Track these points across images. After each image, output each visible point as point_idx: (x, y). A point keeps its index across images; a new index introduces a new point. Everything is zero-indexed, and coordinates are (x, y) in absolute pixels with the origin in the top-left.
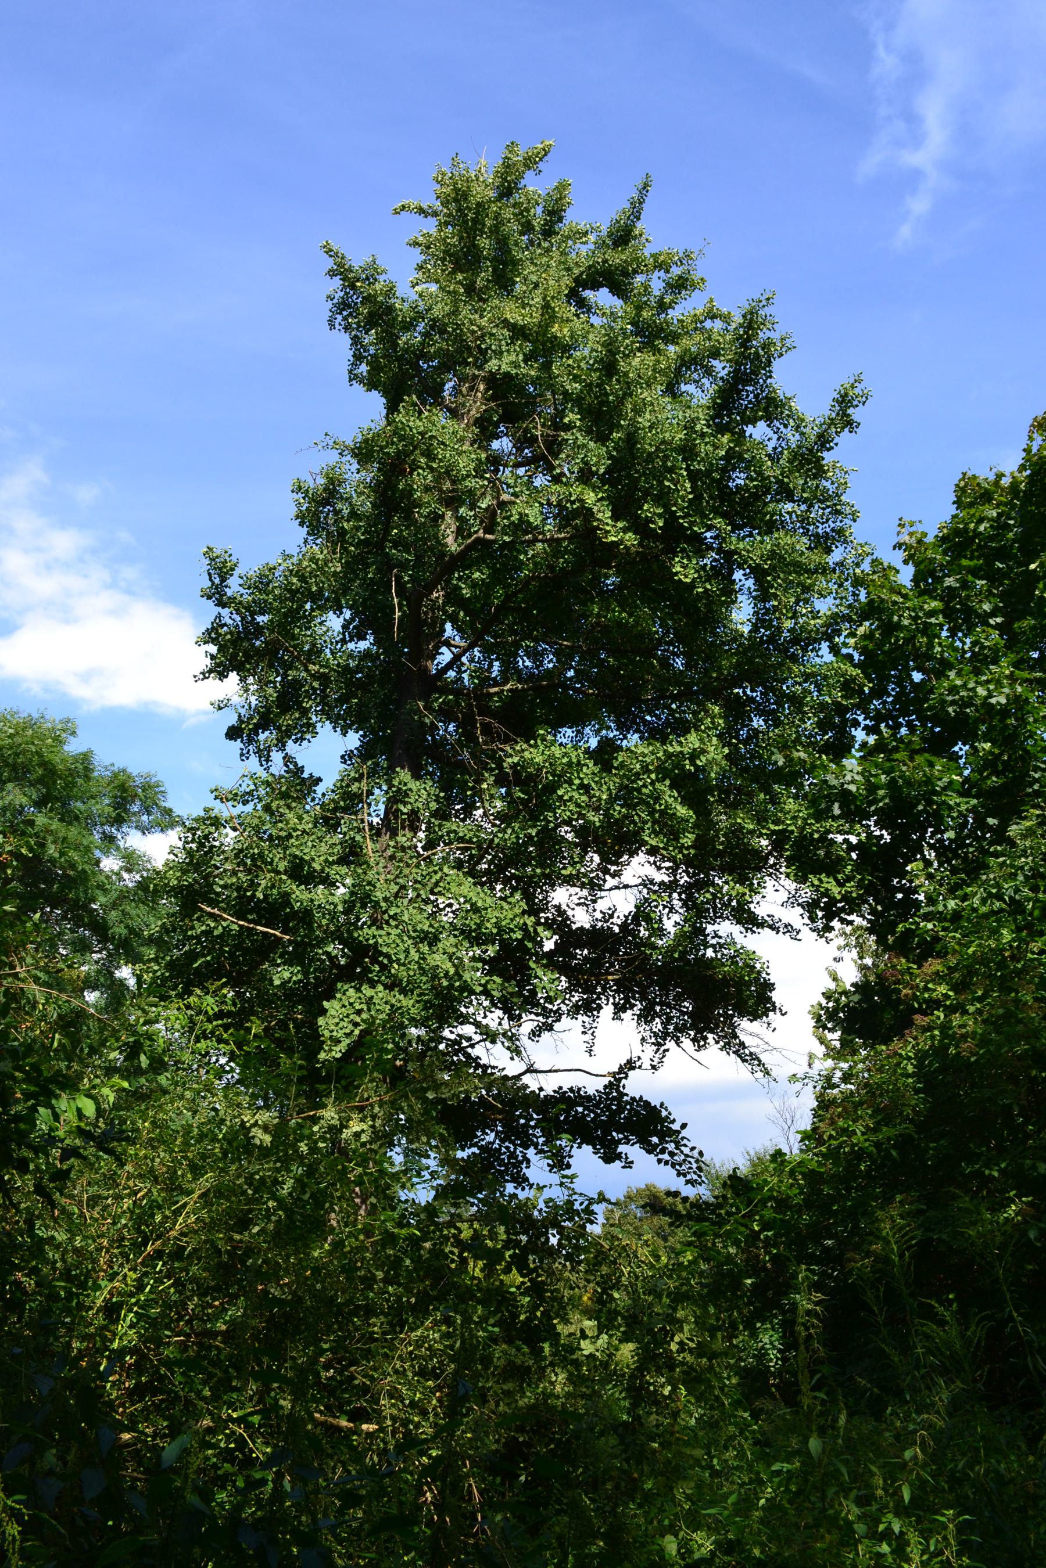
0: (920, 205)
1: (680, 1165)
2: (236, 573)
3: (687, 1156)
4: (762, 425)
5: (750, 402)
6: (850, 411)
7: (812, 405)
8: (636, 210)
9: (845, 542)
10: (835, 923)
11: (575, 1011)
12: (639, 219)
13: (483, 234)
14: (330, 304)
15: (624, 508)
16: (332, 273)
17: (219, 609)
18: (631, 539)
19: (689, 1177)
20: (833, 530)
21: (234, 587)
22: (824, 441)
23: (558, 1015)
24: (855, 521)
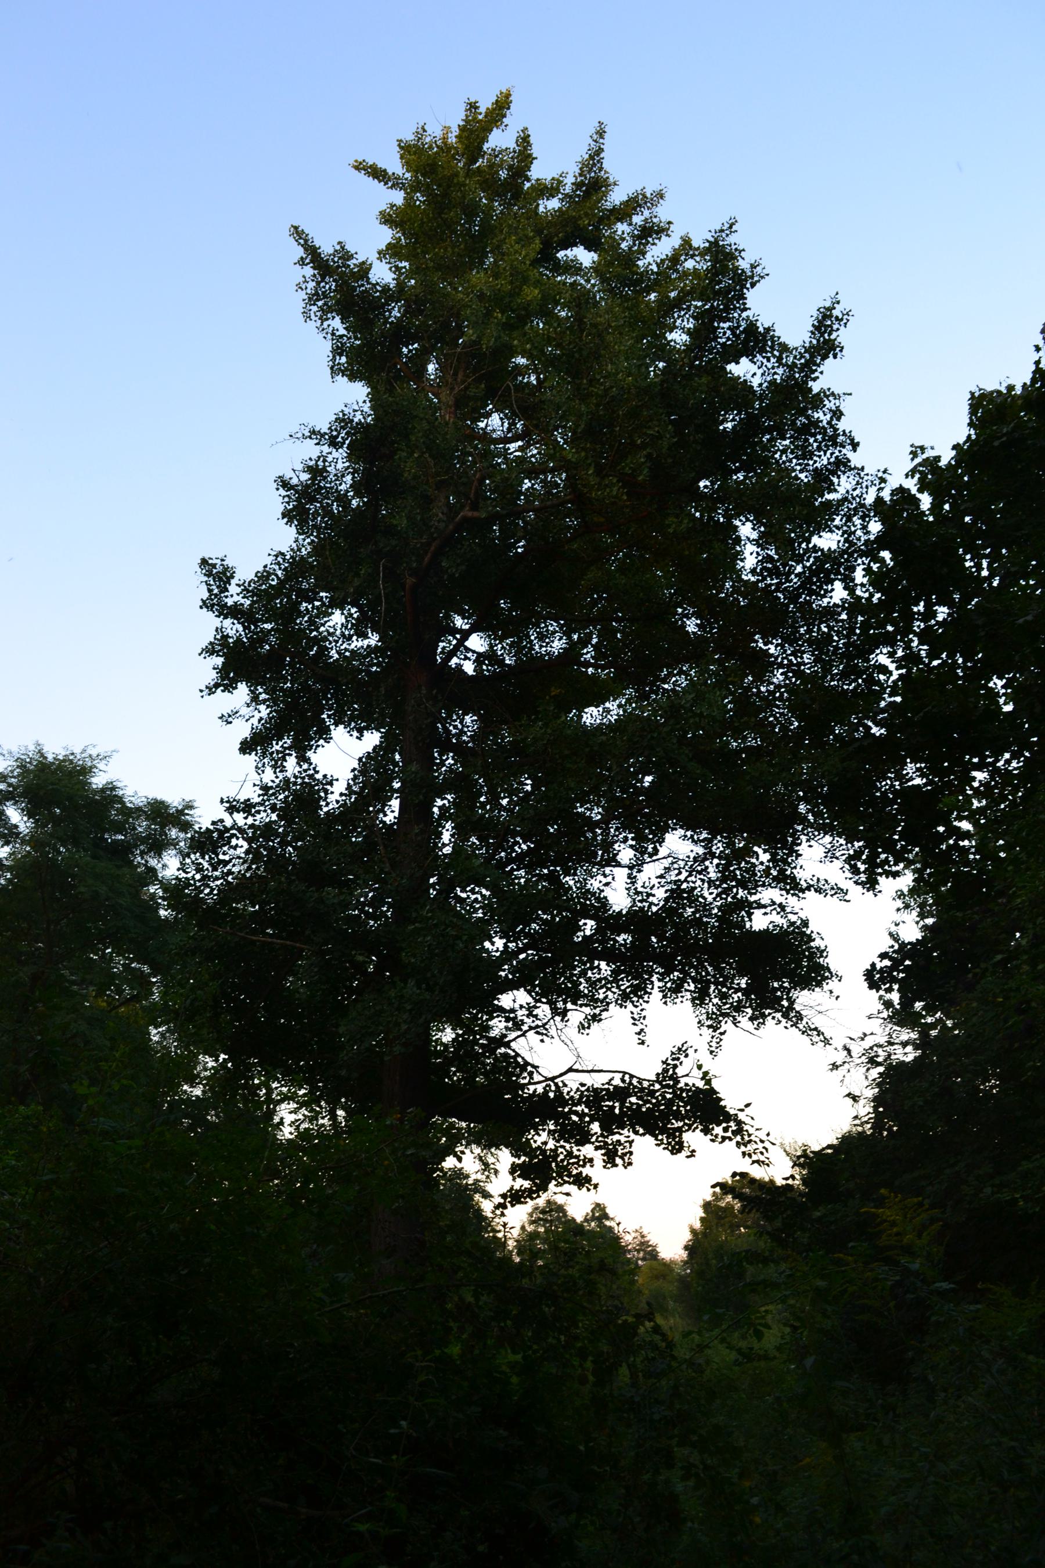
4: (744, 360)
5: (728, 339)
7: (795, 333)
8: (596, 155)
13: (462, 194)
16: (302, 262)
19: (755, 1157)
21: (234, 596)
22: (809, 368)
23: (606, 1004)
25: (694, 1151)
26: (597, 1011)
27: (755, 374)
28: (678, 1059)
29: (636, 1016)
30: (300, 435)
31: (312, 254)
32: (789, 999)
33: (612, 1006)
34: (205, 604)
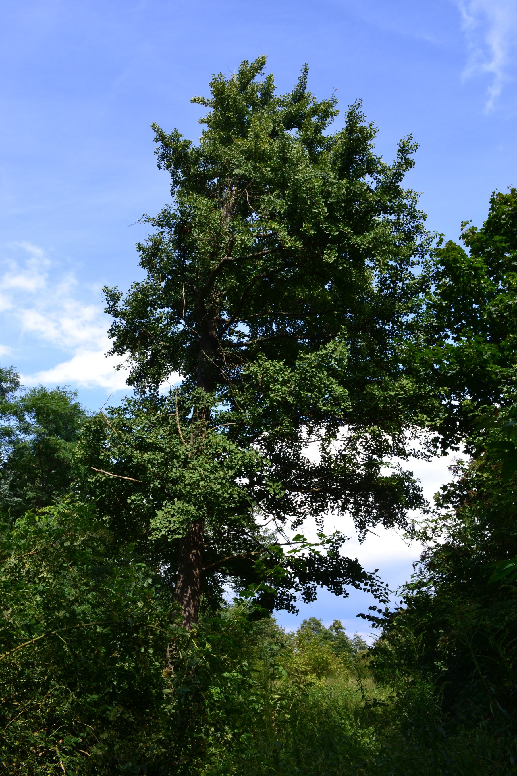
0: (495, 91)
1: (376, 592)
2: (121, 299)
3: (379, 586)
4: (367, 176)
6: (408, 156)
8: (303, 82)
9: (421, 233)
10: (448, 450)
12: (305, 88)
14: (157, 156)
15: (294, 231)
16: (156, 140)
17: (114, 318)
18: (299, 244)
19: (381, 598)
20: (413, 227)
21: (121, 306)
22: (398, 176)
23: (305, 515)
24: (424, 220)
25: (348, 594)
26: (301, 518)
27: (372, 182)
28: (339, 544)
29: (318, 521)
30: (143, 220)
31: (161, 137)
32: (402, 513)
33: (308, 516)
34: (108, 312)
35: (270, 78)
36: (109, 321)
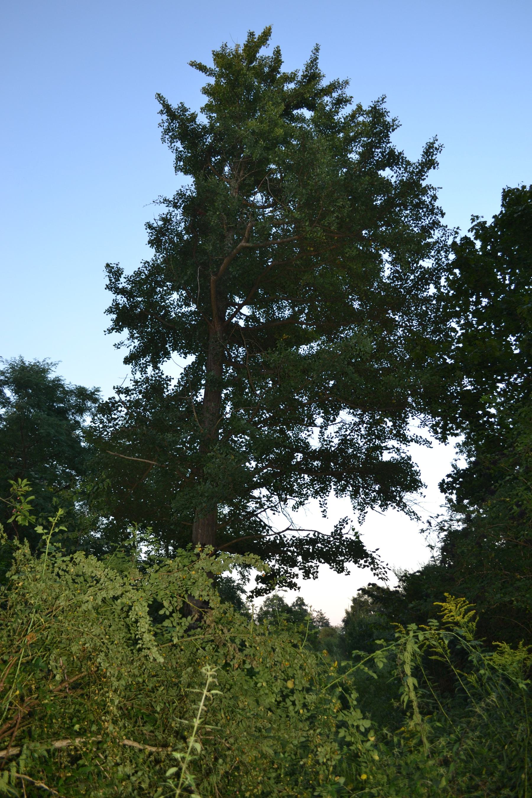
5: (380, 158)
7: (414, 156)
8: (314, 61)
11: (316, 493)
14: (161, 129)
16: (161, 112)
19: (380, 576)
21: (123, 283)
23: (307, 496)
26: (302, 500)
30: (158, 201)
31: (167, 109)
32: (400, 496)
33: (310, 497)
34: (108, 287)
35: (278, 52)
36: (109, 298)
